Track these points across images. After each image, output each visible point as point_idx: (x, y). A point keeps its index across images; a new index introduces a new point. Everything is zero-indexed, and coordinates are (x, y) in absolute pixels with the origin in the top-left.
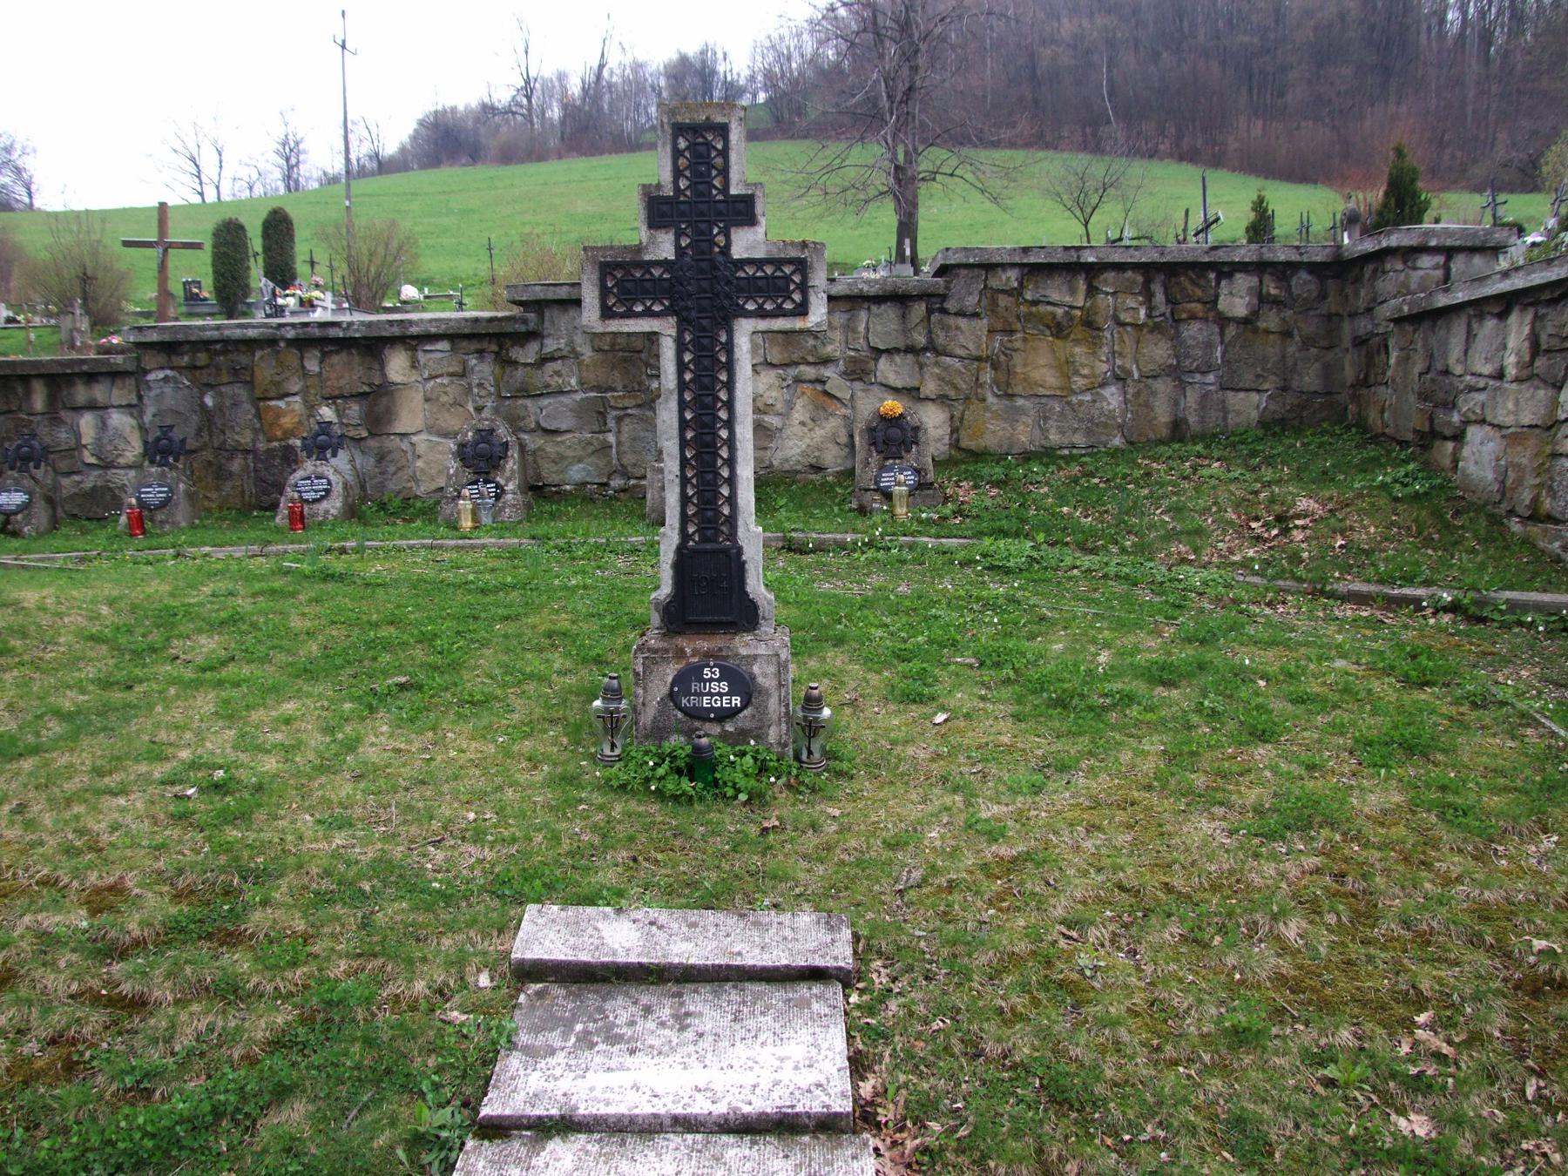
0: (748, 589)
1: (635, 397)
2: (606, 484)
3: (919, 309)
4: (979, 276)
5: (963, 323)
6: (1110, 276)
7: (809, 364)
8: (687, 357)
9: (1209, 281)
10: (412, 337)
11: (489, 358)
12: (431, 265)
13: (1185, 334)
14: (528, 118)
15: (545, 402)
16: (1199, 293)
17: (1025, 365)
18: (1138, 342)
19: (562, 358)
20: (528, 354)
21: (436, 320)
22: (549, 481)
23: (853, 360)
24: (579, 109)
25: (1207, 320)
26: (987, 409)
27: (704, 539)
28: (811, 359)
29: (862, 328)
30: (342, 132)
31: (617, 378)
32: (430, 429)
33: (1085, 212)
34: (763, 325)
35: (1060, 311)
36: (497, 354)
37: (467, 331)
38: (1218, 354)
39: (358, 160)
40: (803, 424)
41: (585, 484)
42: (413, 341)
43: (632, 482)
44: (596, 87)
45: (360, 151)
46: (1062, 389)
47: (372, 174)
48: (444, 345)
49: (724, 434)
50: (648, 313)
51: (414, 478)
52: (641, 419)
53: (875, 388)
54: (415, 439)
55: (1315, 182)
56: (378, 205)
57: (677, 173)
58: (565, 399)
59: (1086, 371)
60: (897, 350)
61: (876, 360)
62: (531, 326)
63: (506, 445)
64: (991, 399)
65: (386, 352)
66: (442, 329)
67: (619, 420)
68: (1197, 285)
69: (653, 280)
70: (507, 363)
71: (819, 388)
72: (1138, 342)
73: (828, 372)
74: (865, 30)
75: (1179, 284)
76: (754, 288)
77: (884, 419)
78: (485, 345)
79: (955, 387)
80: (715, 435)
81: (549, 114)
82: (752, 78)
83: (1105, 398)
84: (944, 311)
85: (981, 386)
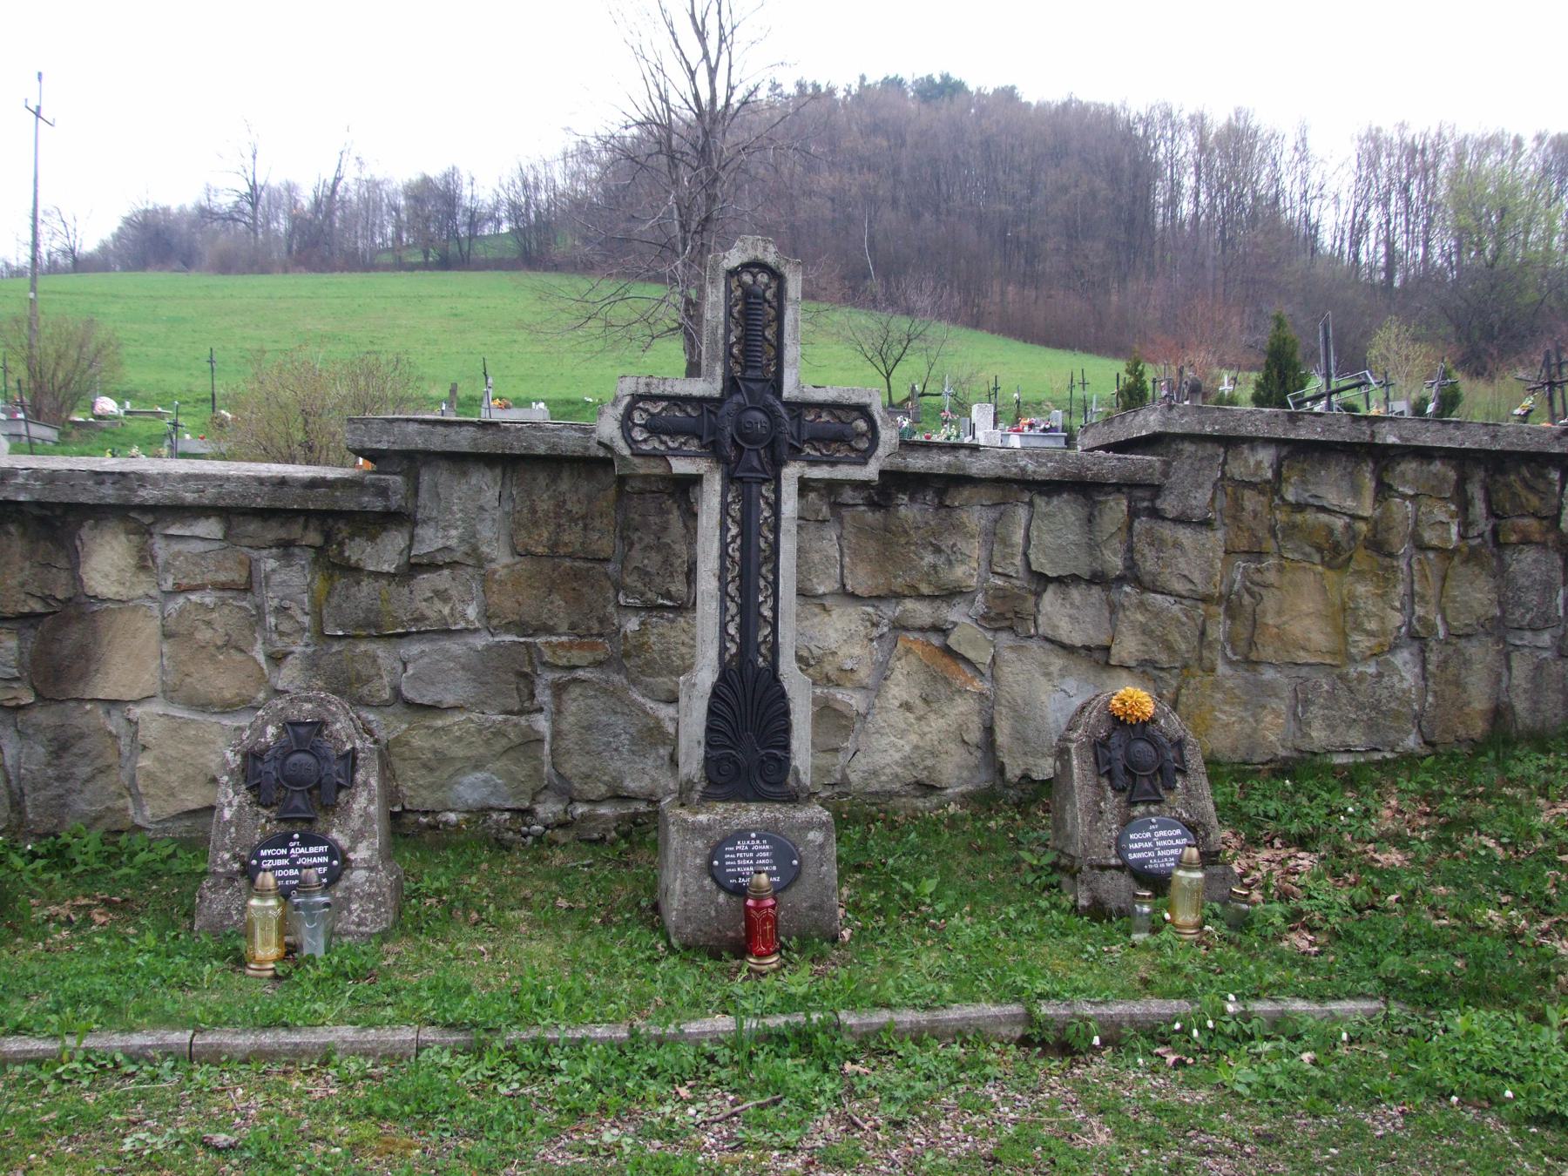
1: (593, 647)
2: (529, 812)
3: (1116, 509)
4: (1212, 457)
5: (1185, 535)
6: (1409, 467)
7: (921, 597)
9: (1550, 483)
10: (144, 508)
11: (303, 558)
12: (134, 376)
13: (1514, 567)
14: (253, 228)
15: (414, 649)
16: (1535, 501)
17: (1279, 613)
18: (1444, 579)
19: (453, 565)
20: (384, 554)
21: (197, 477)
22: (416, 803)
23: (1001, 595)
24: (310, 222)
25: (1543, 545)
26: (1216, 686)
28: (925, 589)
29: (1018, 537)
30: (30, 221)
31: (558, 609)
32: (170, 693)
33: (888, 365)
35: (1339, 523)
36: (320, 550)
37: (260, 503)
38: (1560, 601)
39: (49, 254)
40: (907, 706)
41: (485, 811)
42: (142, 514)
43: (581, 809)
44: (328, 202)
45: (51, 245)
46: (1332, 653)
47: (66, 271)
48: (210, 528)
51: (131, 790)
52: (607, 691)
53: (1033, 645)
54: (137, 712)
55: (1072, 349)
56: (65, 302)
58: (454, 646)
59: (1372, 625)
60: (1075, 579)
61: (1038, 595)
62: (396, 501)
63: (351, 759)
64: (1222, 669)
65: (85, 532)
66: (210, 495)
67: (559, 689)
68: (1531, 489)
70: (336, 568)
71: (936, 640)
72: (1444, 579)
73: (955, 614)
74: (660, 152)
75: (1508, 486)
77: (1117, 722)
78: (296, 531)
79: (1170, 648)
81: (274, 225)
83: (1395, 670)
84: (1156, 514)
85: (1210, 645)
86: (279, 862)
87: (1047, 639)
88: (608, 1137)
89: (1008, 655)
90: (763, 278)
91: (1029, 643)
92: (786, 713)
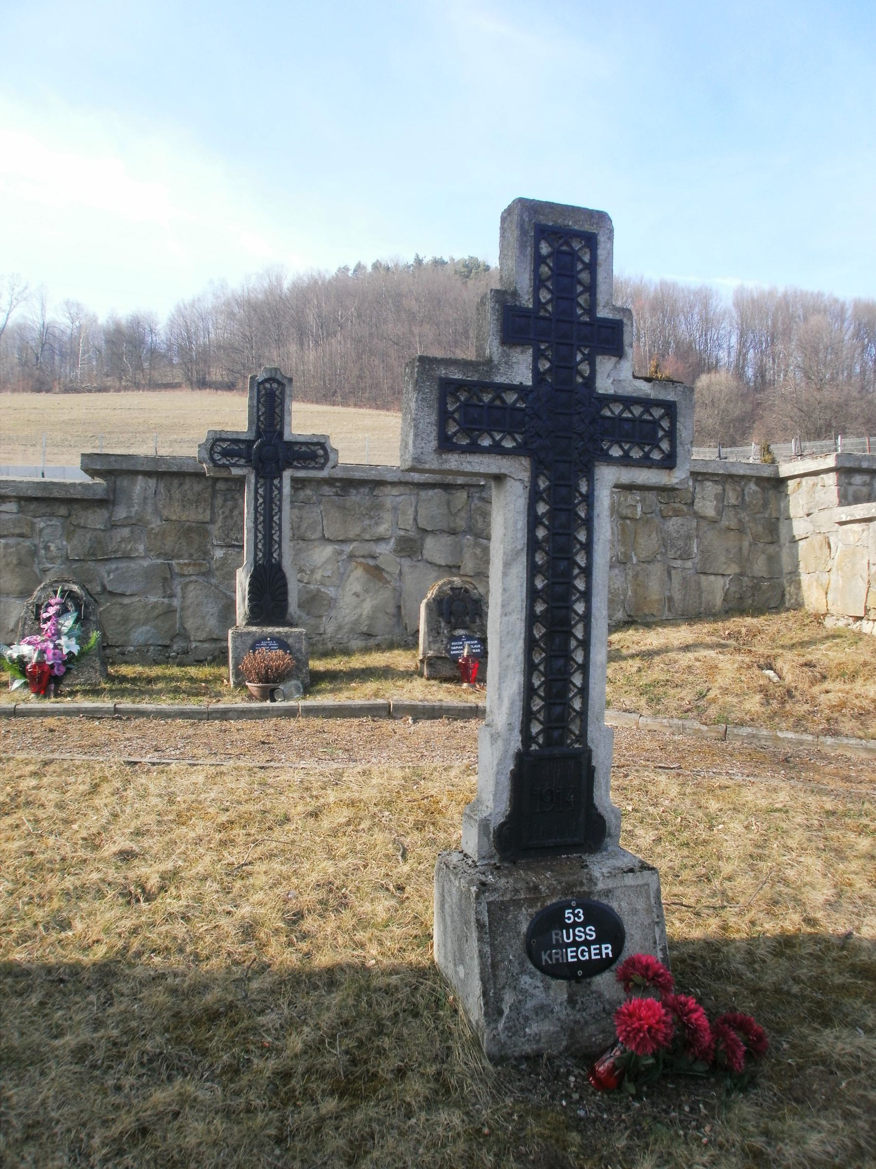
0: (597, 801)
34: (628, 475)
49: (580, 608)
50: (497, 450)
57: (538, 283)
60: (442, 531)
69: (504, 407)
71: (371, 562)
76: (619, 431)
80: (570, 609)
82: (170, 348)
87: (428, 562)
88: (37, 372)
89: (406, 569)
90: (275, 385)
91: (418, 564)
92: (285, 585)
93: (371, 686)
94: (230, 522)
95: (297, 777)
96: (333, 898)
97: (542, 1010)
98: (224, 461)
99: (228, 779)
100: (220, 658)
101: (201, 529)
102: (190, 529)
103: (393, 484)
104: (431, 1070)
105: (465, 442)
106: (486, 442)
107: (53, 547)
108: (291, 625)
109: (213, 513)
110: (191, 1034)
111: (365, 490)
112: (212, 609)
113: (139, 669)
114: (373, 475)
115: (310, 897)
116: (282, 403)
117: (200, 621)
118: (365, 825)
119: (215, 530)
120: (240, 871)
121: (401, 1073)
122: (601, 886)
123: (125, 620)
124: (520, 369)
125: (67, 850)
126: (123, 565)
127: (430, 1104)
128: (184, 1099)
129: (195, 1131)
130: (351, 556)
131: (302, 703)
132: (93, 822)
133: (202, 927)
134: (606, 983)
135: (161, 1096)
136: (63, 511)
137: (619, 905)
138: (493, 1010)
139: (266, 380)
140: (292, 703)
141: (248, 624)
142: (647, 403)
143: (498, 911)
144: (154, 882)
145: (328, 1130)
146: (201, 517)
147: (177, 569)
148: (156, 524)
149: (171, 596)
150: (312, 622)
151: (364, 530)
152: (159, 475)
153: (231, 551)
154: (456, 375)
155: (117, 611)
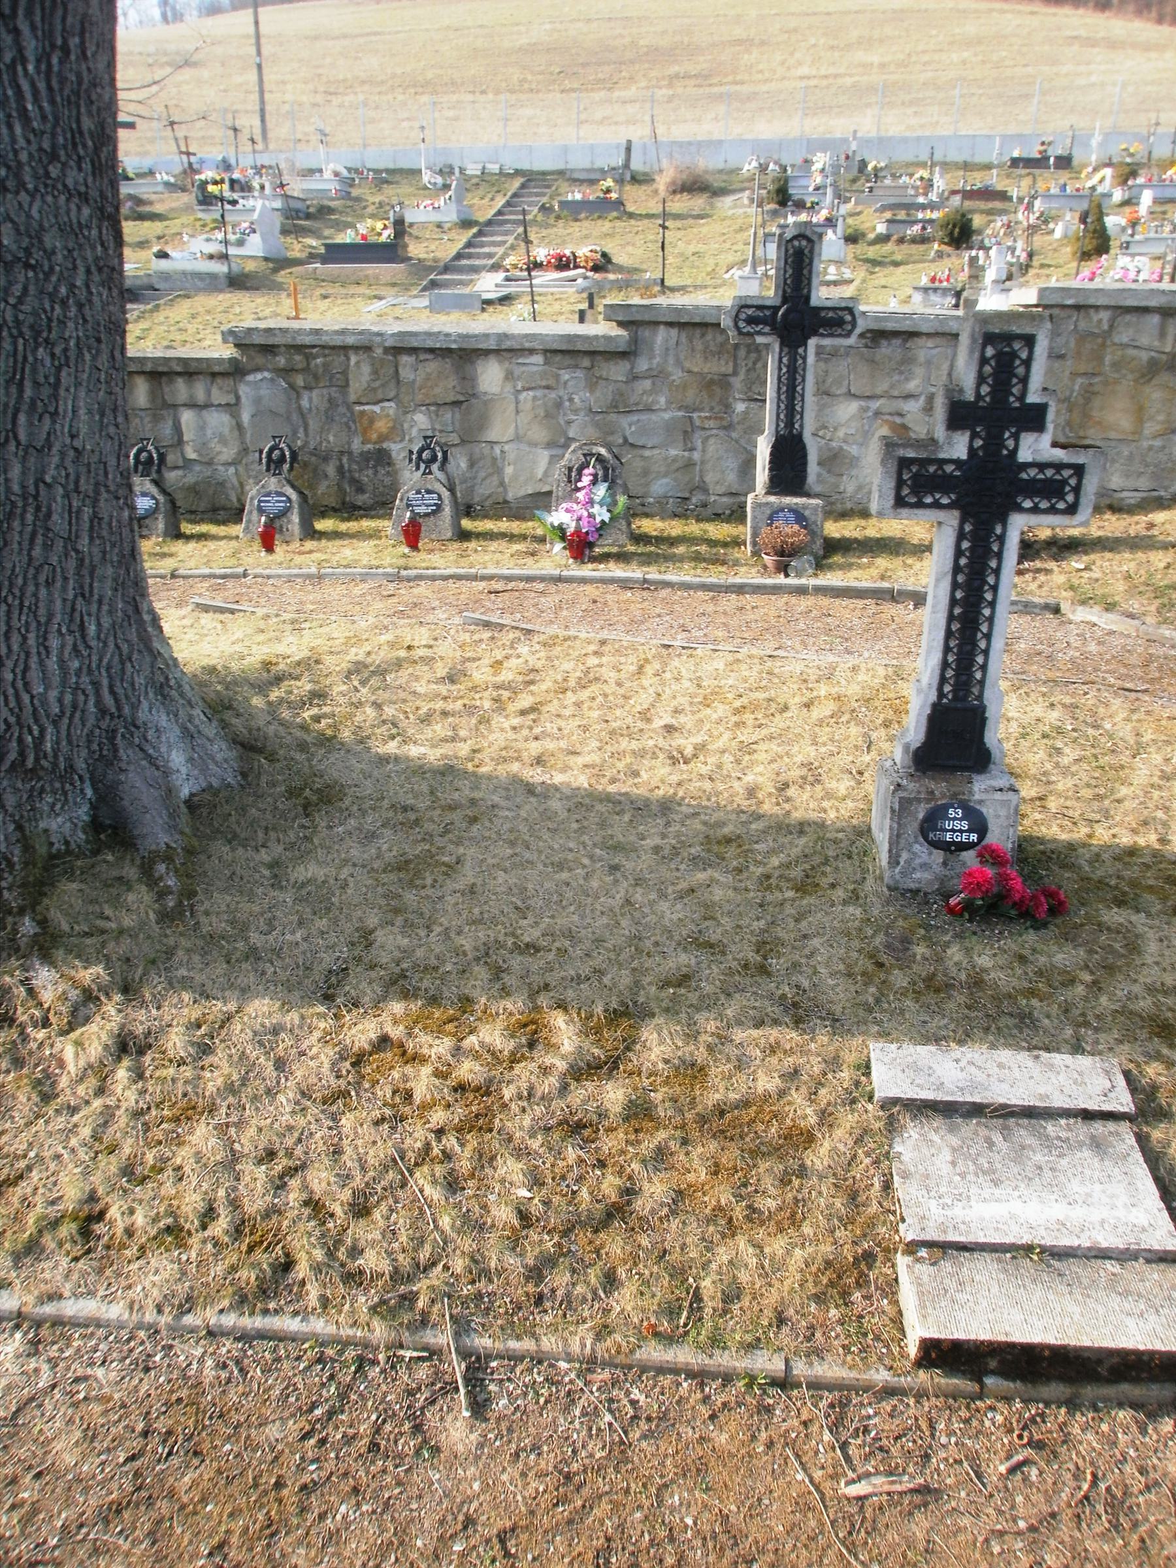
8: (965, 545)
27: (955, 698)
57: (981, 379)
71: (898, 420)
86: (32, 640)
93: (882, 562)
94: (753, 375)
95: (798, 667)
96: (812, 776)
97: (925, 866)
98: (749, 329)
99: (744, 667)
100: (737, 515)
101: (723, 382)
102: (712, 382)
103: (928, 335)
104: (851, 887)
105: (913, 500)
106: (929, 500)
107: (576, 399)
108: (808, 495)
109: (735, 366)
110: (715, 848)
111: (897, 342)
112: (731, 464)
113: (659, 524)
114: (906, 326)
115: (796, 773)
116: (811, 263)
117: (720, 475)
118: (845, 718)
119: (737, 382)
120: (748, 748)
121: (833, 886)
122: (977, 797)
123: (646, 472)
124: (959, 447)
125: (629, 720)
126: (644, 417)
127: (845, 903)
128: (712, 879)
129: (718, 894)
130: (877, 413)
131: (813, 582)
132: (642, 700)
133: (721, 787)
134: (969, 858)
135: (701, 876)
136: (586, 362)
137: (987, 811)
138: (894, 861)
139: (795, 238)
140: (803, 581)
141: (768, 493)
142: (1059, 466)
143: (905, 804)
144: (689, 751)
145: (787, 905)
146: (723, 370)
147: (698, 423)
148: (677, 375)
149: (692, 449)
150: (832, 479)
151: (892, 386)
152: (681, 326)
153: (753, 405)
154: (911, 454)
155: (638, 464)
